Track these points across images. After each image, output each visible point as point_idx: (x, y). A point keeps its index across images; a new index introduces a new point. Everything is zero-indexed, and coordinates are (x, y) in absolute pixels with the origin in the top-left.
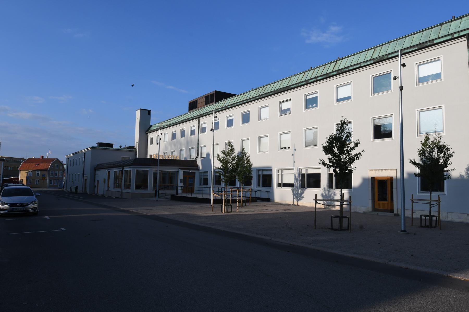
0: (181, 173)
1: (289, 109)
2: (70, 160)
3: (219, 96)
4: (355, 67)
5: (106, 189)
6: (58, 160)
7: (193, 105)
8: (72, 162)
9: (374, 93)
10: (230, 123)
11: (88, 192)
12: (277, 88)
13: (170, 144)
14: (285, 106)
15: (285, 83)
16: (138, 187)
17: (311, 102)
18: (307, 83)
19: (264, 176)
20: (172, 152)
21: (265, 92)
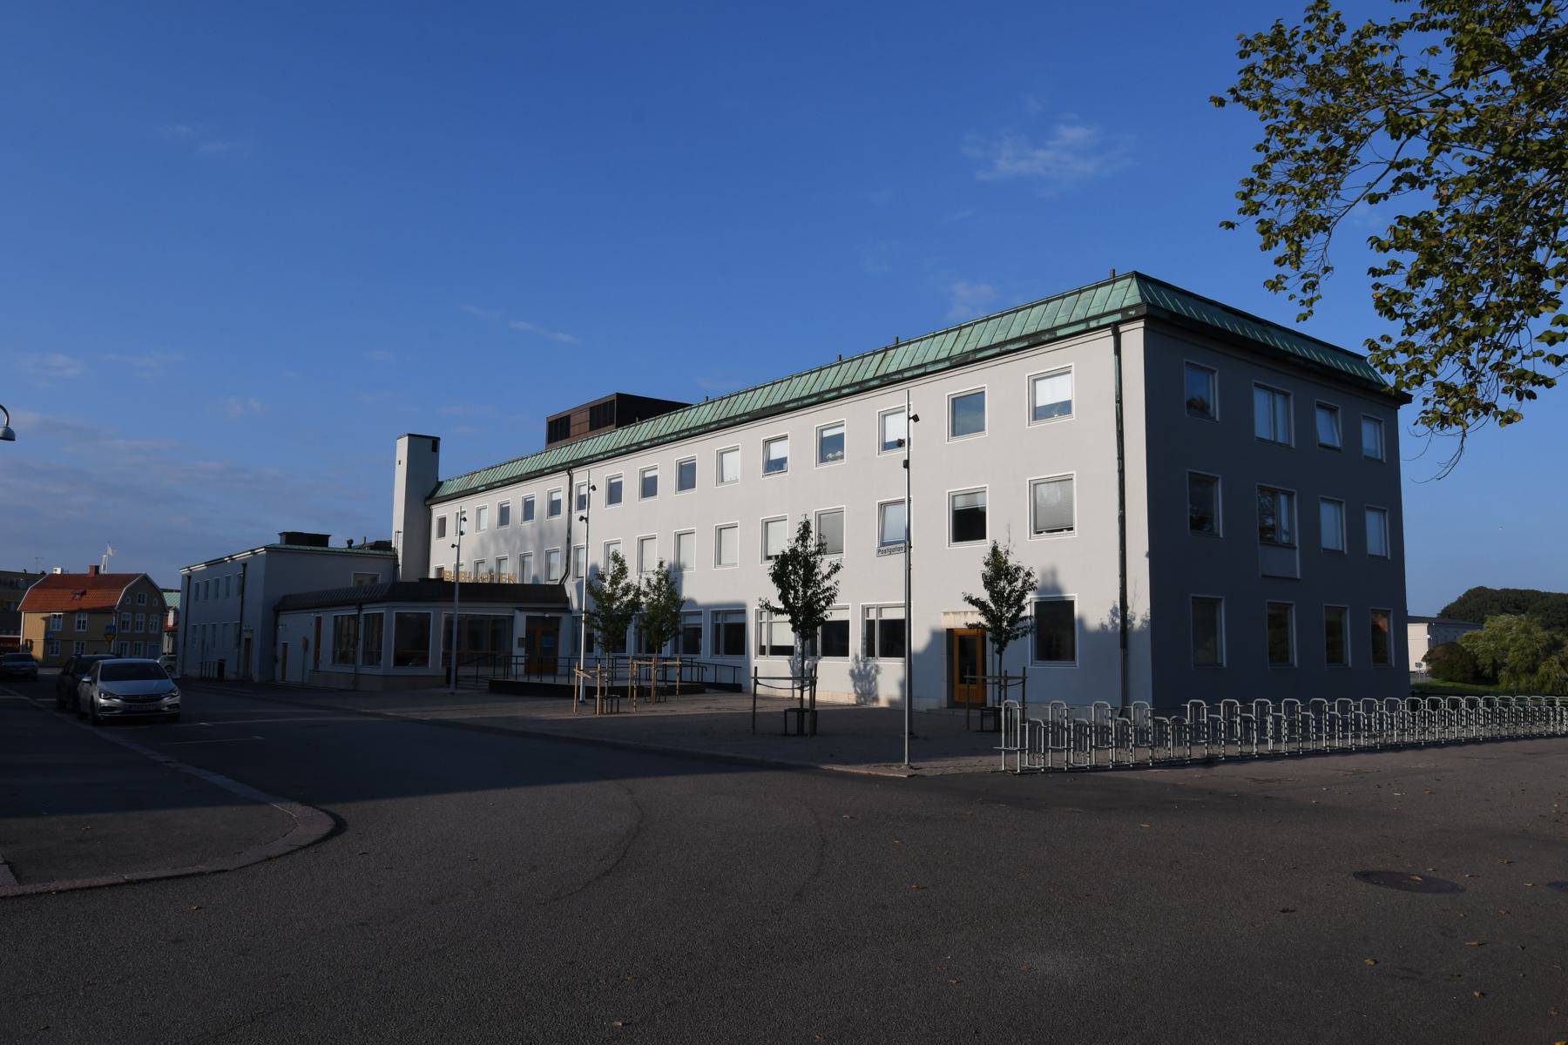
0: (521, 620)
1: (784, 460)
2: (194, 581)
3: (628, 409)
4: (916, 372)
5: (311, 666)
6: (145, 578)
7: (559, 430)
8: (202, 589)
9: (954, 434)
10: (649, 487)
11: (256, 678)
12: (758, 406)
13: (495, 537)
14: (777, 451)
15: (778, 395)
16: (400, 660)
17: (830, 447)
18: (821, 399)
19: (729, 627)
20: (499, 561)
21: (732, 414)
